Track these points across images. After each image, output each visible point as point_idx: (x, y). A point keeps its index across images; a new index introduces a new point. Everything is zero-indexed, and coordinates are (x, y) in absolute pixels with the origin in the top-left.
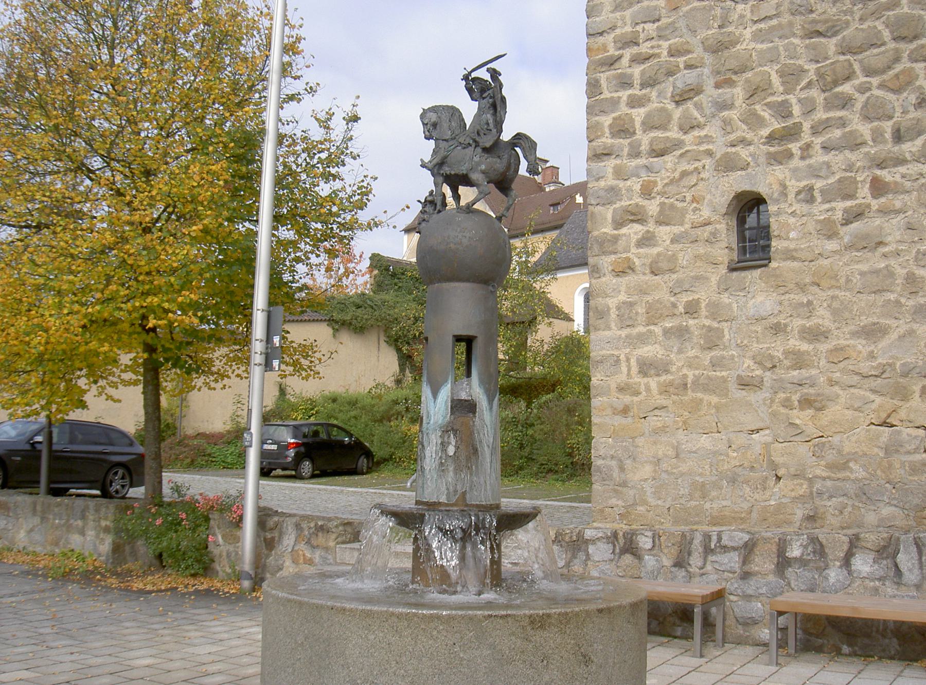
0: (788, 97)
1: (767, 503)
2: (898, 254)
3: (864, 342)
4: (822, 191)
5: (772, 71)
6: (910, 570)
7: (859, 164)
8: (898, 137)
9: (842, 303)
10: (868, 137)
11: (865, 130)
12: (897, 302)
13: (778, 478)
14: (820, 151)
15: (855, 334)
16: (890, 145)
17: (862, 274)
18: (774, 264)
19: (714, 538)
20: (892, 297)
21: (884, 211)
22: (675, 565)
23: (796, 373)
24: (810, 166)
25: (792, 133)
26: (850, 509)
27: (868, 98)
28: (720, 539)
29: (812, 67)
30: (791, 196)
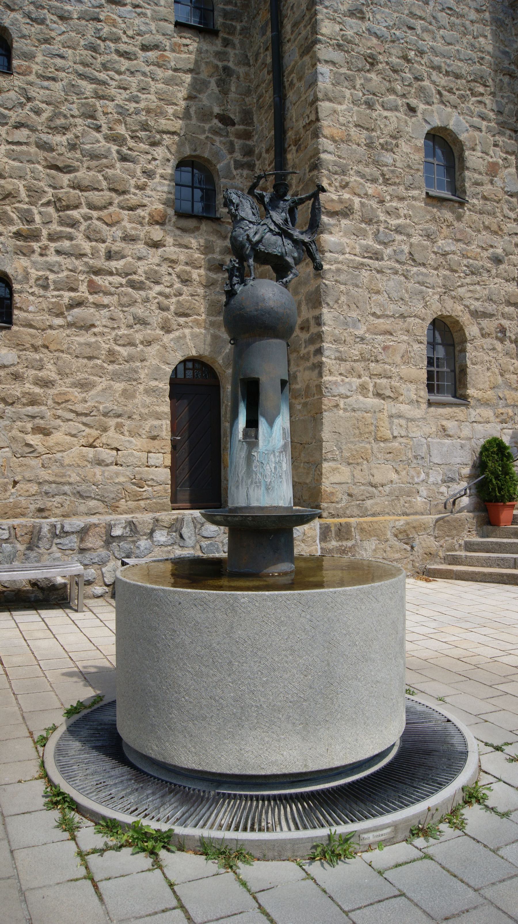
0: (32, 207)
1: (7, 501)
2: (103, 334)
3: (79, 390)
4: (54, 282)
5: (20, 185)
6: (189, 538)
7: (80, 268)
8: (110, 256)
9: (64, 362)
10: (88, 251)
11: (86, 246)
12: (102, 367)
13: (15, 483)
14: (54, 253)
15: (74, 385)
16: (103, 260)
17: (80, 344)
18: (15, 328)
19: (59, 526)
20: (99, 362)
21: (98, 306)
22: (28, 549)
23: (30, 408)
24: (47, 262)
25: (35, 236)
26: (68, 503)
27: (90, 225)
28: (63, 527)
29: (50, 191)
30: (32, 282)
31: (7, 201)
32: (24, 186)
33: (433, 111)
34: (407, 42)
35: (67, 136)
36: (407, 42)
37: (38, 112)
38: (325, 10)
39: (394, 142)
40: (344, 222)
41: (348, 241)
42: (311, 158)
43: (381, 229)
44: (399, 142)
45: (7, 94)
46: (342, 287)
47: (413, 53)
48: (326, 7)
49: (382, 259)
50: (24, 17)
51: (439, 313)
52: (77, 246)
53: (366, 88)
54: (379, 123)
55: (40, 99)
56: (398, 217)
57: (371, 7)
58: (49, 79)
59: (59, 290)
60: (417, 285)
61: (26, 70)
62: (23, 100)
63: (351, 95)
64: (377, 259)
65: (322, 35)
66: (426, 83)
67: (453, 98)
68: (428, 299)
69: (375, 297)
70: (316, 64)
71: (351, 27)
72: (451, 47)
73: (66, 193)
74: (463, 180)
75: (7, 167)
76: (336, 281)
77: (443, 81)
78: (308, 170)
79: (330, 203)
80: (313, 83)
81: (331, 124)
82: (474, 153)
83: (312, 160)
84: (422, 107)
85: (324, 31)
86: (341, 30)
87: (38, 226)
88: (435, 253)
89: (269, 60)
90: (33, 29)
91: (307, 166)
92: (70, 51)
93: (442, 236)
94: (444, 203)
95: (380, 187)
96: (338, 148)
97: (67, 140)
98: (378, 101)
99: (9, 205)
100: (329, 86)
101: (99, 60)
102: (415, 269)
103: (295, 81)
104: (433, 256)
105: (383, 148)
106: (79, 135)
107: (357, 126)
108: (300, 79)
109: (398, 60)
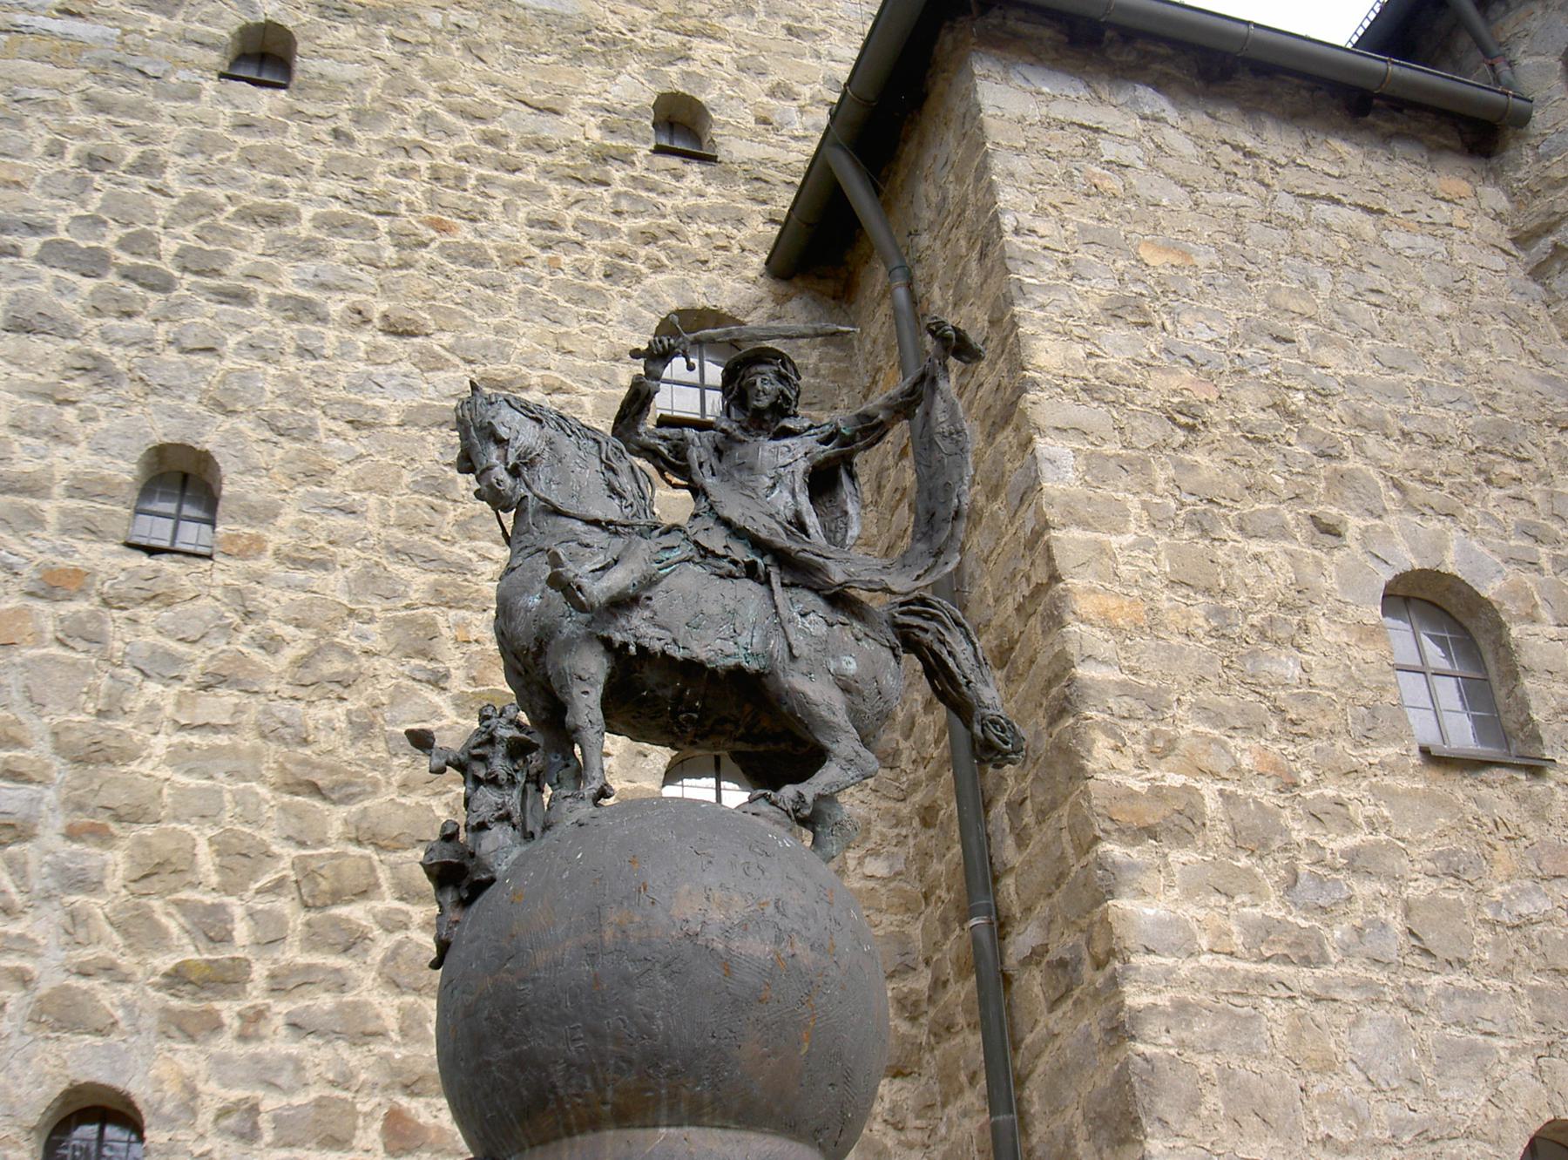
0: (226, 899)
4: (278, 1120)
5: (202, 839)
7: (363, 1076)
10: (391, 1021)
14: (283, 1031)
25: (228, 979)
27: (400, 945)
29: (290, 852)
30: (206, 1118)
31: (156, 884)
32: (211, 841)
33: (1387, 531)
34: (1277, 374)
35: (348, 705)
36: (1277, 374)
37: (271, 644)
38: (1038, 314)
39: (1296, 620)
40: (1179, 856)
41: (1201, 914)
42: (1050, 684)
43: (1303, 867)
44: (1309, 618)
45: (189, 606)
46: (1205, 1063)
47: (1301, 396)
48: (1042, 307)
49: (1324, 960)
50: (259, 425)
51: (1548, 1117)
52: (356, 1006)
53: (1184, 486)
54: (1238, 572)
55: (279, 614)
56: (1349, 825)
57: (1164, 300)
58: (307, 564)
59: (291, 1145)
60: (1454, 1031)
61: (249, 547)
62: (235, 619)
63: (1145, 506)
64: (1306, 961)
65: (1039, 369)
66: (1354, 463)
67: (1436, 496)
68: (1498, 1071)
69: (1319, 1086)
70: (1030, 440)
71: (1119, 349)
72: (1400, 376)
73: (334, 856)
74: (1524, 705)
75: (166, 791)
76: (1182, 1043)
77: (1398, 457)
78: (1044, 723)
79: (1125, 804)
80: (1032, 486)
81: (1096, 584)
82: (1537, 628)
83: (1054, 691)
84: (1354, 524)
85: (1041, 359)
86: (1090, 355)
87: (240, 954)
88: (1493, 925)
89: (910, 478)
90: (279, 453)
91: (1041, 713)
92: (373, 500)
93: (1499, 871)
94: (1484, 775)
95: (1275, 748)
96: (1126, 648)
97: (349, 713)
98: (1225, 517)
99: (161, 895)
100: (1077, 488)
101: (451, 516)
102: (1435, 981)
103: (981, 500)
104: (1483, 934)
105: (1263, 636)
106: (384, 699)
107: (1173, 584)
108: (993, 493)
109: (1262, 415)
